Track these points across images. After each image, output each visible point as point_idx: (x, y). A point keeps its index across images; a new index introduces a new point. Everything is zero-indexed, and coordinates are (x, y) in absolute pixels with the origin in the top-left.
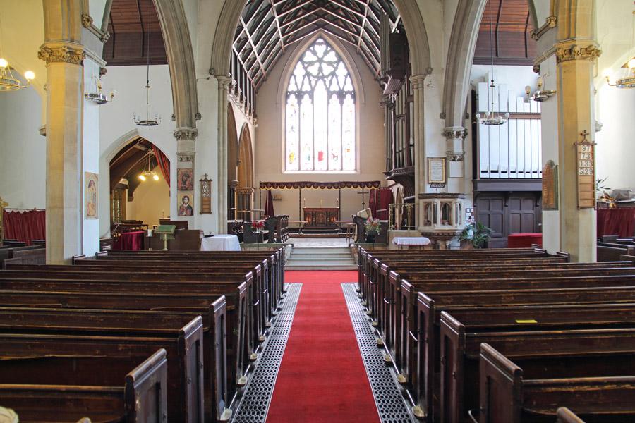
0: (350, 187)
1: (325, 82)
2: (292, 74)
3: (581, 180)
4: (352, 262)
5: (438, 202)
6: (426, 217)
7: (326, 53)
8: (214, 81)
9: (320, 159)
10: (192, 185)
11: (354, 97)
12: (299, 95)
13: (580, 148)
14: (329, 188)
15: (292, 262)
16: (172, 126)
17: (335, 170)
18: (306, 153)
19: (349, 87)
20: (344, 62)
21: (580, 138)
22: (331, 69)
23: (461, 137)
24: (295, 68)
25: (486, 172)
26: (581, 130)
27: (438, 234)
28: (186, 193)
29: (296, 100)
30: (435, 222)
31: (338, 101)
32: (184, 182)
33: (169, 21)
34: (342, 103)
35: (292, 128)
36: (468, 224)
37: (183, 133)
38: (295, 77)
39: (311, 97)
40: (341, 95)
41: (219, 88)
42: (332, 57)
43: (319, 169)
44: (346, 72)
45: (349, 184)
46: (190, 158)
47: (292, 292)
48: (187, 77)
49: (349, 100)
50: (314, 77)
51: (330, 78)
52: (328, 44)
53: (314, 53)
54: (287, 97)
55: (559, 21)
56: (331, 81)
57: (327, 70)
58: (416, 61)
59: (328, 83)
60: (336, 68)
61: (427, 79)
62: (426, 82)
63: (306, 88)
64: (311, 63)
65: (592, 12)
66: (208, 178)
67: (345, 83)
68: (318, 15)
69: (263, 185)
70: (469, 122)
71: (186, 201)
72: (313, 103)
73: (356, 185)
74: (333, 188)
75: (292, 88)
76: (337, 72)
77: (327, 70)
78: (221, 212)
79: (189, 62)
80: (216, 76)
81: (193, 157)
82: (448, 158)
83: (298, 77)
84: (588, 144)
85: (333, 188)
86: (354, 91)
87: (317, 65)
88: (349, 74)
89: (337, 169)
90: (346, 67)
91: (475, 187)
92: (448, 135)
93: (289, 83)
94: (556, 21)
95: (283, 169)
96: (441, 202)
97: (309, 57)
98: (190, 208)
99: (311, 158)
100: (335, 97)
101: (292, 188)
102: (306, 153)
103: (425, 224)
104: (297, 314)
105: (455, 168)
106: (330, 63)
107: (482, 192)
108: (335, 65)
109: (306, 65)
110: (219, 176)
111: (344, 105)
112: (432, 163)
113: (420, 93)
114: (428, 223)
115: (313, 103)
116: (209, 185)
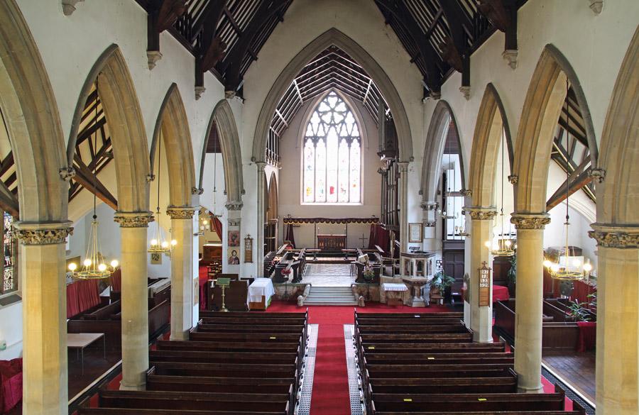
1: (336, 128)
2: (309, 122)
3: (482, 290)
4: (353, 299)
5: (414, 260)
6: (406, 269)
7: (338, 103)
8: (255, 166)
10: (239, 242)
11: (360, 141)
12: (315, 139)
13: (482, 272)
15: (310, 299)
16: (223, 199)
18: (320, 187)
19: (356, 134)
20: (352, 113)
21: (482, 266)
22: (341, 118)
23: (433, 210)
24: (312, 116)
25: (451, 235)
26: (482, 261)
27: (414, 283)
28: (234, 248)
29: (313, 144)
30: (412, 274)
32: (233, 241)
33: (225, 133)
34: (349, 146)
35: (309, 167)
36: (438, 272)
37: (233, 206)
38: (312, 124)
39: (325, 141)
40: (349, 140)
41: (258, 171)
42: (342, 107)
44: (353, 121)
46: (238, 223)
47: (313, 331)
48: (236, 166)
49: (355, 143)
50: (328, 125)
51: (340, 125)
52: (339, 96)
53: (328, 104)
54: (305, 141)
55: (473, 194)
56: (341, 128)
57: (338, 118)
58: (402, 147)
59: (338, 129)
60: (345, 117)
61: (410, 165)
62: (409, 167)
63: (321, 134)
64: (325, 113)
65: (492, 189)
66: (250, 237)
67: (352, 130)
68: (332, 76)
70: (440, 197)
71: (234, 253)
72: (326, 146)
75: (309, 133)
76: (346, 121)
77: (338, 118)
78: (260, 261)
79: (237, 156)
80: (256, 163)
81: (239, 223)
82: (424, 224)
83: (314, 125)
84: (486, 269)
86: (360, 137)
87: (330, 114)
88: (356, 122)
90: (354, 116)
91: (443, 247)
92: (424, 207)
93: (307, 130)
94: (471, 194)
95: (301, 199)
96: (417, 261)
97: (323, 107)
98: (237, 259)
100: (344, 141)
101: (309, 223)
102: (320, 187)
103: (405, 274)
104: (317, 360)
105: (429, 232)
106: (341, 113)
108: (345, 114)
109: (321, 114)
110: (258, 235)
112: (413, 228)
113: (405, 175)
114: (407, 273)
115: (326, 146)
116: (251, 242)
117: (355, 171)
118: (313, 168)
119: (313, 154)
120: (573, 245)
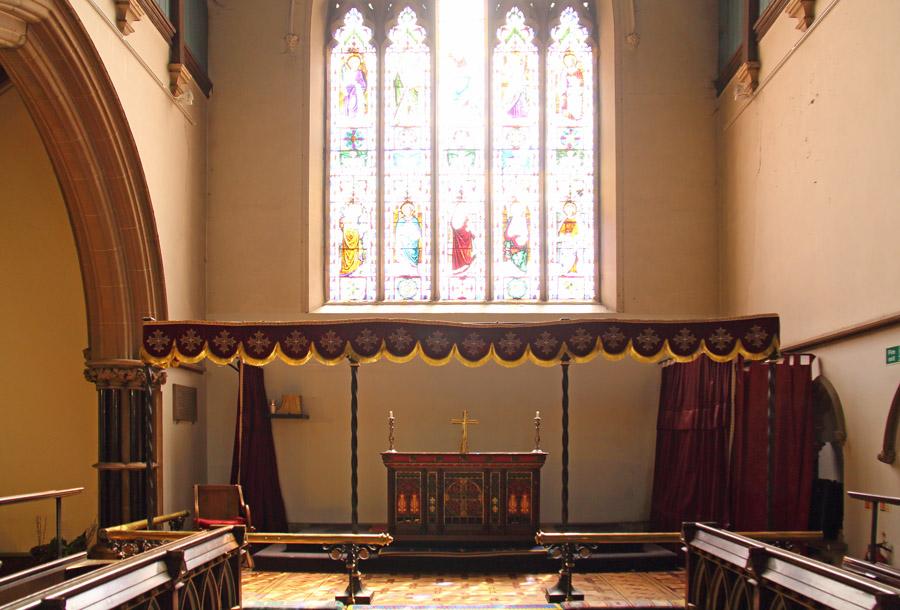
0: (515, 356)
9: (461, 257)
14: (616, 349)
17: (517, 300)
18: (404, 236)
31: (530, 36)
34: (543, 41)
43: (564, 296)
45: (615, 336)
69: (158, 340)
72: (430, 41)
73: (648, 339)
74: (529, 357)
85: (529, 357)
89: (470, 296)
99: (426, 256)
102: (404, 236)
107: (486, 353)
111: (502, 49)
115: (430, 41)
117: (569, 160)
118: (370, 142)
119: (372, 79)
120: (305, 425)
